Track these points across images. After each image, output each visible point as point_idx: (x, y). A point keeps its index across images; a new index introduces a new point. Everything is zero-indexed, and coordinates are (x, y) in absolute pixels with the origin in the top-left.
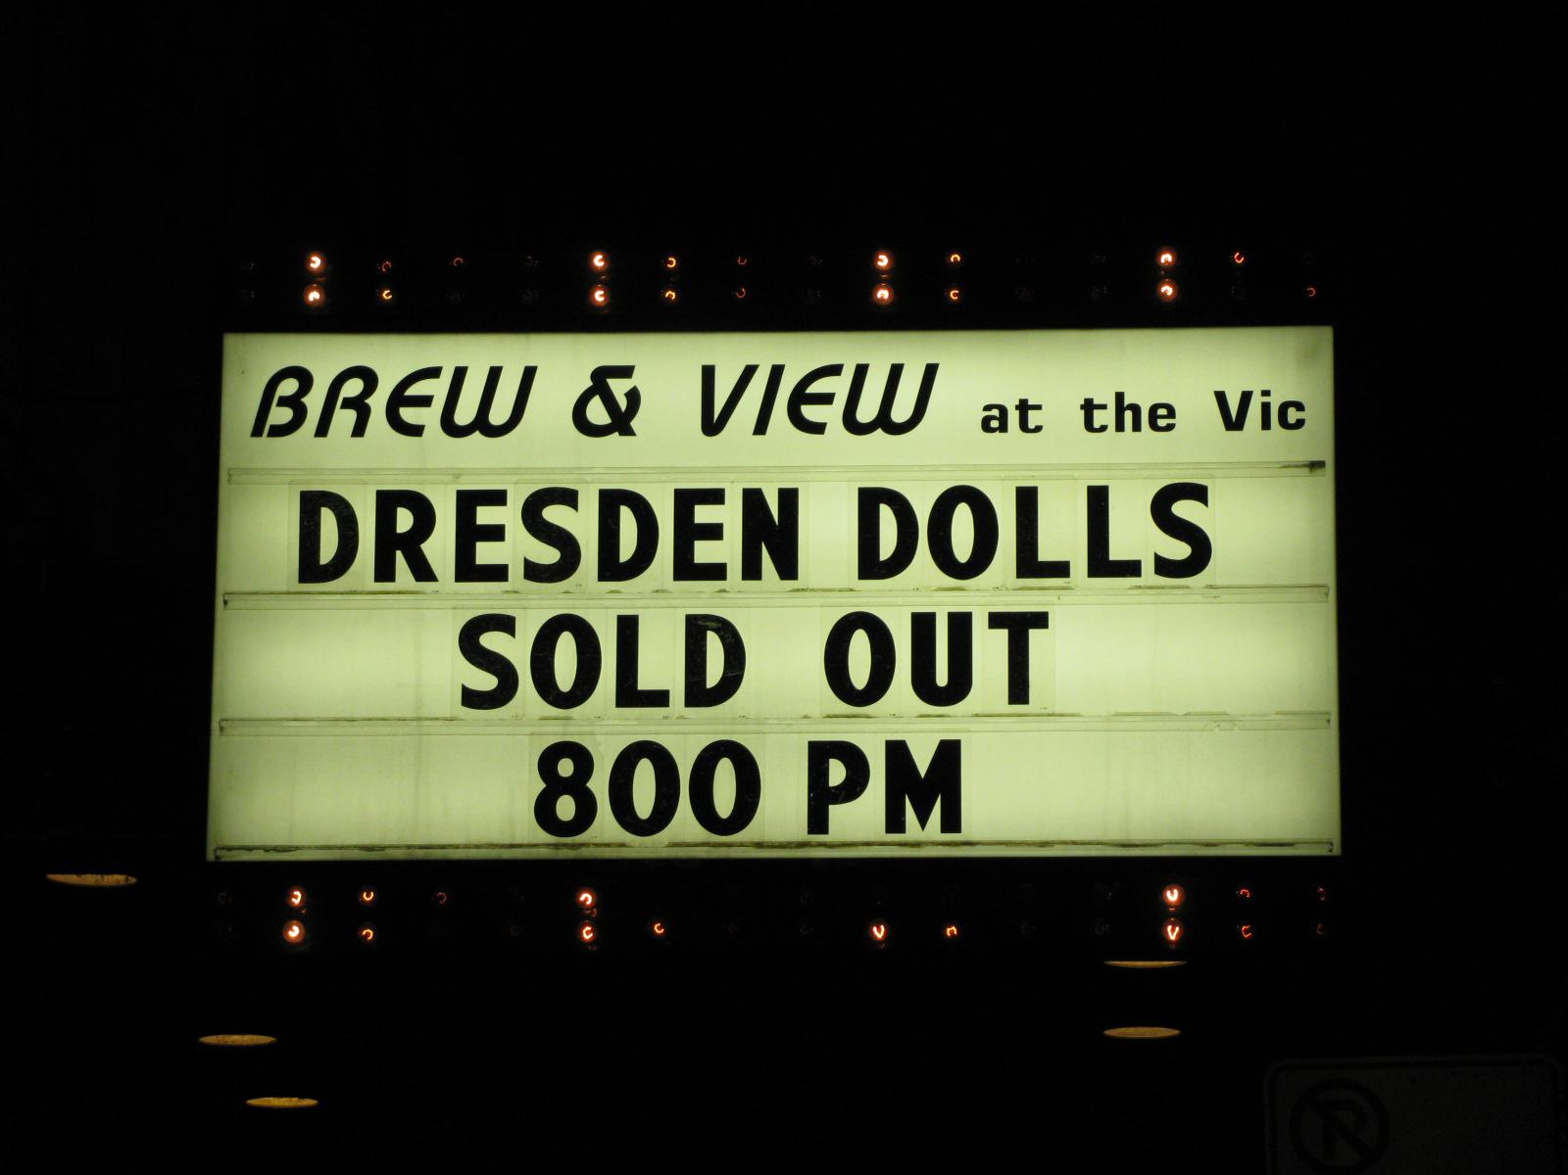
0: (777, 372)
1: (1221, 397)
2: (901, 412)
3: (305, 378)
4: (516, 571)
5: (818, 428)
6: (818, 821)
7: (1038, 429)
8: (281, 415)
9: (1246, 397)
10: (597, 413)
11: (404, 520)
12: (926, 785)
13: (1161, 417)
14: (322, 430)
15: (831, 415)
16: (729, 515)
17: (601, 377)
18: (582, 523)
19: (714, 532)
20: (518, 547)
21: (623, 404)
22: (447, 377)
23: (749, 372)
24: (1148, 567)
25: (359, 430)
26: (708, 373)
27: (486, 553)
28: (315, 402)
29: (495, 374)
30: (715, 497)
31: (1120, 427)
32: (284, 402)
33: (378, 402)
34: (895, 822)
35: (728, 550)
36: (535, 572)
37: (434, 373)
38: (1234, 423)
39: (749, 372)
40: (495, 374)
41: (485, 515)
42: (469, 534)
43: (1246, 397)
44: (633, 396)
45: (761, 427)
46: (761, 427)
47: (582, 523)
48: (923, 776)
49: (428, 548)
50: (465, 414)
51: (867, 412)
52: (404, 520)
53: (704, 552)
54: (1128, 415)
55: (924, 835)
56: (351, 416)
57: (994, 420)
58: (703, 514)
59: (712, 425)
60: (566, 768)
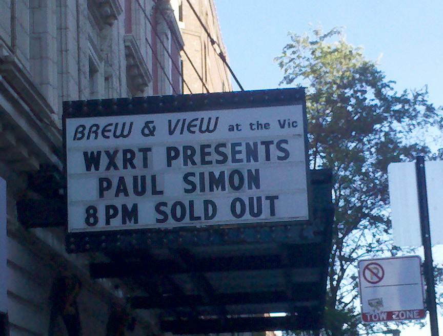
0: (184, 120)
1: (279, 121)
2: (211, 128)
3: (84, 127)
4: (214, 162)
5: (194, 132)
6: (108, 223)
7: (240, 130)
8: (79, 135)
9: (285, 121)
10: (147, 131)
11: (129, 156)
12: (131, 214)
13: (267, 126)
14: (88, 138)
15: (196, 129)
16: (243, 148)
17: (147, 123)
18: (228, 151)
19: (240, 152)
20: (215, 157)
21: (152, 129)
22: (114, 125)
23: (179, 121)
24: (214, 162)
25: (96, 138)
26: (170, 121)
27: (207, 158)
28: (86, 132)
29: (124, 124)
30: (240, 144)
31: (258, 129)
32: (80, 132)
33: (100, 131)
34: (124, 222)
35: (243, 156)
36: (218, 162)
37: (197, 119)
38: (282, 126)
39: (179, 121)
40: (124, 124)
41: (207, 150)
42: (204, 154)
43: (285, 121)
44: (154, 128)
45: (181, 133)
46: (181, 133)
47: (228, 151)
48: (130, 210)
49: (135, 162)
50: (118, 133)
51: (118, 133)
52: (189, 152)
53: (238, 157)
54: (260, 126)
55: (130, 225)
56: (94, 135)
57: (231, 129)
58: (238, 148)
59: (171, 132)
60: (91, 211)
